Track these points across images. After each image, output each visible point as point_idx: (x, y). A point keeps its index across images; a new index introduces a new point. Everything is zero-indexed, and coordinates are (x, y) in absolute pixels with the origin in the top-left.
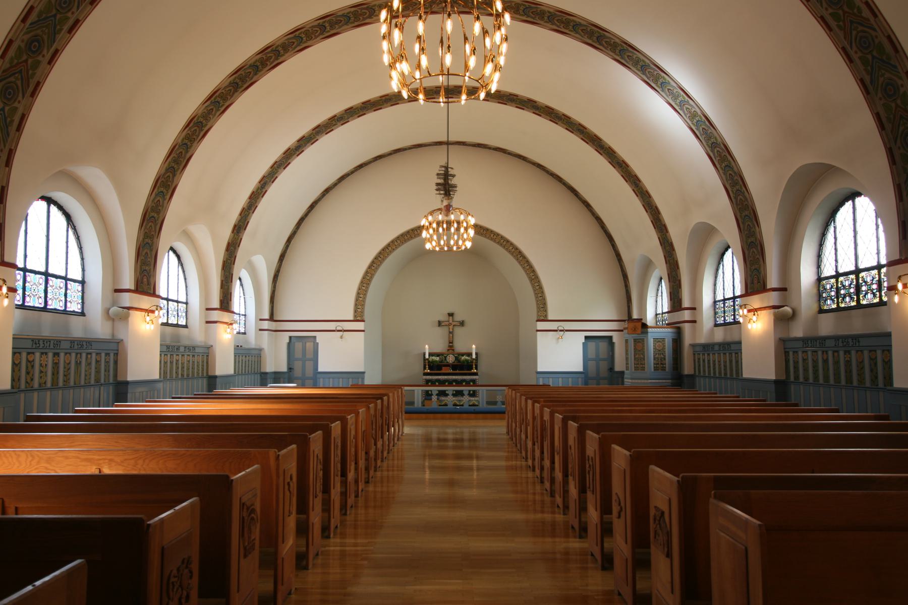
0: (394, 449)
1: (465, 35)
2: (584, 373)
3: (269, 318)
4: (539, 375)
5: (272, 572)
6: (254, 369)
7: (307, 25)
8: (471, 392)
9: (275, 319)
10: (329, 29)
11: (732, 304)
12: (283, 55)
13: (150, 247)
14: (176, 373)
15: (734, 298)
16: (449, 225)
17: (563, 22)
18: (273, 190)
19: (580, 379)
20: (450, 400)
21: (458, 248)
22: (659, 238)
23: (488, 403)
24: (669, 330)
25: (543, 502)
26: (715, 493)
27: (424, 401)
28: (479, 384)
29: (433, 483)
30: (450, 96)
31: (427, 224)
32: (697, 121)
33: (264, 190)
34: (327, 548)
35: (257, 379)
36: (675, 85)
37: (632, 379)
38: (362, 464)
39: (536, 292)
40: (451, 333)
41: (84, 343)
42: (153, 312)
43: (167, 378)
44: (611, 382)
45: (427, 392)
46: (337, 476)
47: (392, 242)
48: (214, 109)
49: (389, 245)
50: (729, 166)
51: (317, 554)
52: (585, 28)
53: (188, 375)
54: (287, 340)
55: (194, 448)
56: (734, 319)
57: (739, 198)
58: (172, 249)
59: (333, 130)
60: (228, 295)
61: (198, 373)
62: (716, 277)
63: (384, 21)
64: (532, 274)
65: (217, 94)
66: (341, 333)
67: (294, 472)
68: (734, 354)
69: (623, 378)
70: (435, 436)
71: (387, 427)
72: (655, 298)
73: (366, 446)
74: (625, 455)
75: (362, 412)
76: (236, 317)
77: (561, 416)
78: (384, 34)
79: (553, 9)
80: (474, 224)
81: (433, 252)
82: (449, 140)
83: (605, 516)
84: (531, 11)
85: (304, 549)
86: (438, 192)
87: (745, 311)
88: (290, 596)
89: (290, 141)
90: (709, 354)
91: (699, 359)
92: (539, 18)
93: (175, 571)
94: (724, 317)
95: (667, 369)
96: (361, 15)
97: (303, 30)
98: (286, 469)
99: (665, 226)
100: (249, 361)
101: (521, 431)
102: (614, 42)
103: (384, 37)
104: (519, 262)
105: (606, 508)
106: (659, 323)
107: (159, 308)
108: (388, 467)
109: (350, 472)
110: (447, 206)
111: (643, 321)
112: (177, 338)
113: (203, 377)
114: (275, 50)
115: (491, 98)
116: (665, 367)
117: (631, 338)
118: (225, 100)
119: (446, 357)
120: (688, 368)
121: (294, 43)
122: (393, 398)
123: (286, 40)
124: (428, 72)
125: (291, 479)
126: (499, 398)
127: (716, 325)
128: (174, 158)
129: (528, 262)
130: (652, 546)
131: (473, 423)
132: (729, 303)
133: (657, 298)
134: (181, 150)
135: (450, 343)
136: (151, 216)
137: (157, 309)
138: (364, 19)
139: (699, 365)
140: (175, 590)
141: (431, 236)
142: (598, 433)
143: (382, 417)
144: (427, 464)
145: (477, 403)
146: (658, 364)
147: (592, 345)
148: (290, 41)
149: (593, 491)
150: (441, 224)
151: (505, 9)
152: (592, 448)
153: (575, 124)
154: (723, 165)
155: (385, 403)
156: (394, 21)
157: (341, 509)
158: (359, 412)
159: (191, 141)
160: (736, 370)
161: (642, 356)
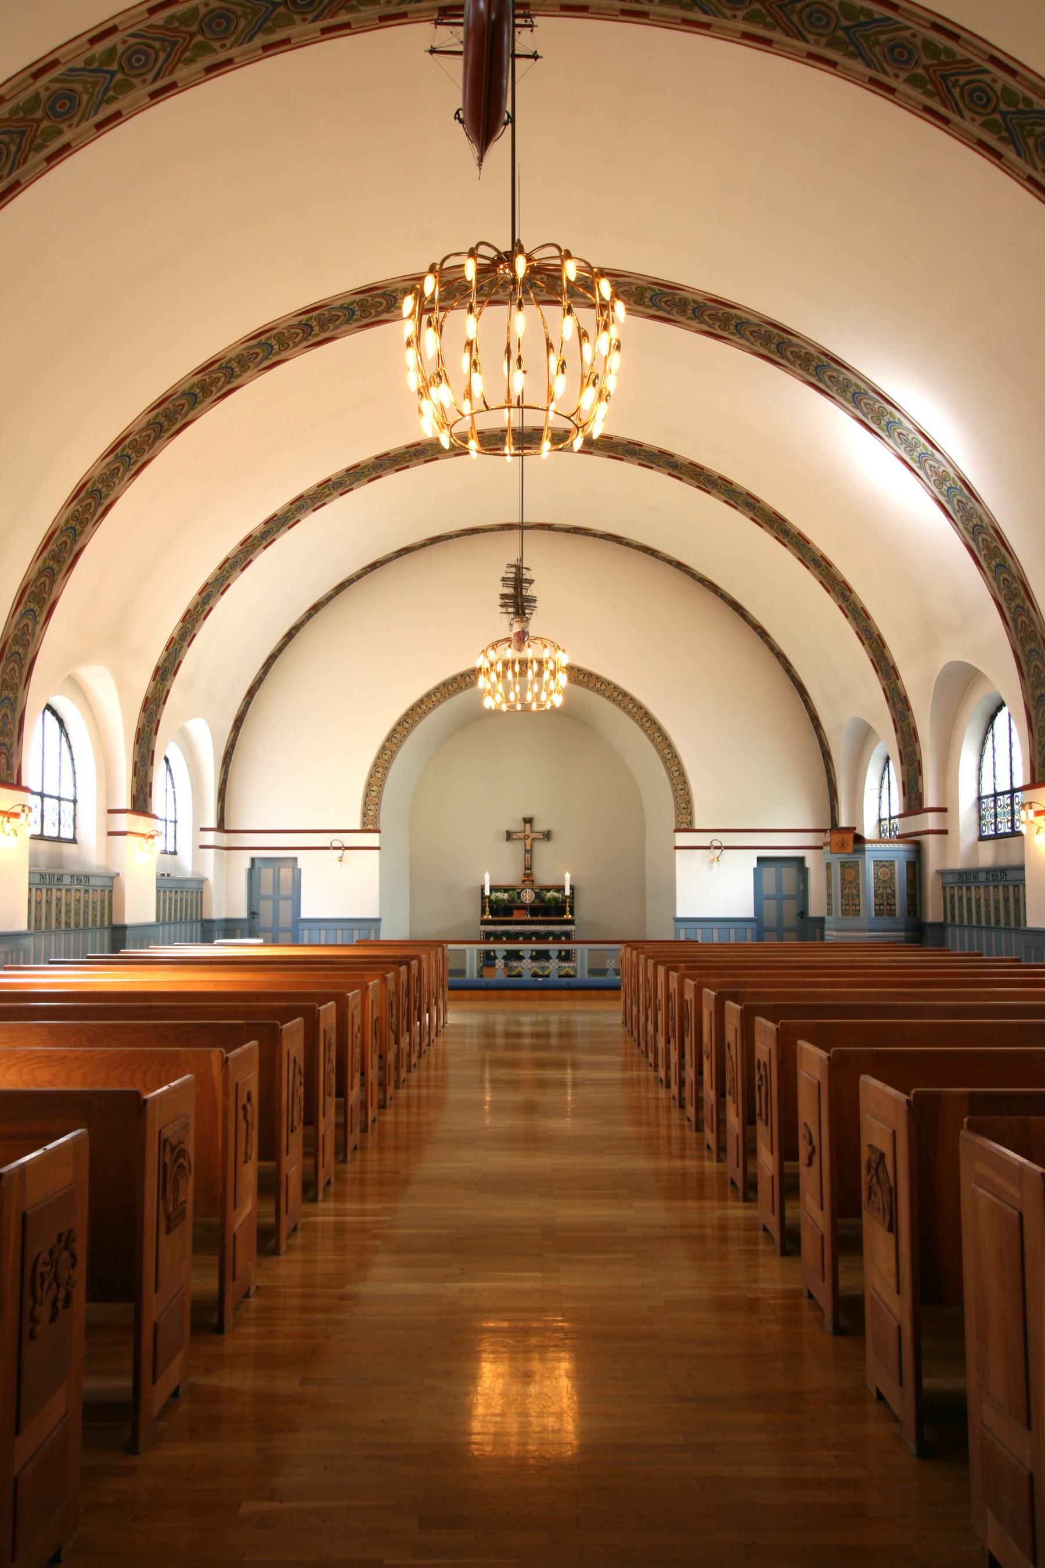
0: (429, 1050)
1: (547, 340)
2: (758, 920)
3: (216, 827)
4: (680, 925)
5: (215, 1259)
6: (191, 913)
7: (281, 323)
8: (563, 953)
9: (226, 828)
10: (317, 332)
11: (1009, 801)
12: (240, 375)
13: (12, 704)
14: (57, 920)
15: (1012, 792)
16: (524, 666)
17: (718, 319)
18: (223, 606)
19: (749, 932)
20: (527, 966)
21: (540, 706)
22: (884, 689)
23: (592, 972)
24: (901, 846)
25: (683, 1140)
26: (968, 1121)
27: (482, 968)
28: (577, 939)
29: (497, 1108)
30: (525, 446)
31: (486, 665)
32: (949, 488)
33: (208, 608)
34: (312, 1219)
35: (196, 931)
36: (910, 427)
37: (837, 930)
38: (373, 1075)
39: (674, 782)
40: (529, 852)
41: (83, 878)
42: (16, 815)
43: (40, 929)
44: (802, 936)
45: (487, 953)
46: (330, 1095)
47: (428, 695)
48: (122, 469)
49: (421, 701)
50: (1003, 566)
51: (295, 1229)
52: (756, 329)
53: (77, 925)
54: (247, 865)
55: (84, 1047)
56: (1013, 827)
57: (1020, 621)
58: (49, 707)
59: (324, 504)
60: (146, 787)
61: (94, 922)
62: (981, 756)
63: (410, 317)
64: (666, 751)
65: (126, 442)
66: (340, 852)
67: (254, 1087)
68: (1011, 888)
69: (822, 929)
70: (500, 1028)
71: (416, 1012)
72: (877, 792)
73: (381, 1042)
74: (821, 1058)
75: (374, 986)
76: (160, 825)
77: (713, 993)
78: (408, 339)
79: (701, 295)
80: (567, 665)
81: (497, 712)
82: (524, 521)
83: (786, 1164)
84: (664, 300)
85: (273, 1220)
86: (504, 610)
87: (1031, 812)
88: (247, 1300)
89: (252, 522)
90: (968, 888)
91: (952, 896)
92: (677, 312)
93: (45, 1255)
94: (995, 824)
95: (898, 913)
96: (372, 306)
97: (274, 332)
98: (239, 1083)
99: (894, 668)
100: (181, 900)
101: (647, 1019)
102: (806, 353)
103: (409, 344)
104: (645, 731)
105: (788, 1151)
106: (885, 835)
107: (26, 809)
108: (419, 1081)
109: (352, 1089)
110: (519, 633)
111: (857, 831)
112: (58, 860)
113: (102, 927)
114: (226, 367)
115: (595, 449)
116: (895, 910)
117: (836, 860)
118: (140, 452)
119: (519, 894)
120: (933, 912)
121: (257, 354)
122: (428, 961)
123: (244, 350)
124: (485, 402)
125: (249, 1099)
126: (611, 964)
127: (982, 838)
128: (53, 552)
129: (659, 729)
130: (865, 1215)
131: (565, 1006)
132: (1004, 801)
133: (881, 791)
134: (64, 539)
135: (526, 869)
136: (13, 651)
137: (23, 811)
138: (378, 314)
139: (953, 907)
140: (46, 1286)
141: (494, 686)
142: (775, 1021)
143: (408, 995)
144: (487, 1075)
145: (572, 973)
146: (883, 904)
147: (769, 872)
148: (252, 351)
149: (767, 1121)
150: (510, 665)
151: (615, 295)
152: (764, 1047)
153: (740, 493)
154: (994, 563)
155: (414, 971)
156: (425, 318)
157: (337, 1153)
158: (368, 986)
159: (81, 522)
160: (1015, 916)
161: (854, 891)
